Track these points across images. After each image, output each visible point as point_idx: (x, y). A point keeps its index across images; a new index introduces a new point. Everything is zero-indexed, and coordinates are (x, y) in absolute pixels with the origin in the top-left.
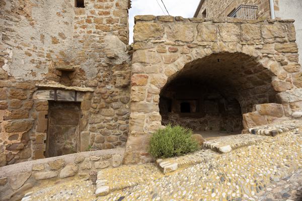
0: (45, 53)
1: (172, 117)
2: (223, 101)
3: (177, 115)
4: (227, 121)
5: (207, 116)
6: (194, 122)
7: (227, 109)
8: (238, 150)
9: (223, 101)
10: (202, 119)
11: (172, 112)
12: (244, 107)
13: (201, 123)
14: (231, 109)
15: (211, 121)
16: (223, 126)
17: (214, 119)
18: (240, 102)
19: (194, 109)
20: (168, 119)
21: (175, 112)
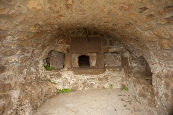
0: (25, 110)
1: (65, 75)
2: (127, 54)
3: (71, 73)
4: (130, 79)
5: (107, 72)
6: (92, 79)
7: (131, 64)
8: (134, 99)
9: (127, 54)
10: (102, 76)
11: (66, 69)
12: (158, 76)
13: (100, 79)
14: (135, 65)
15: (113, 77)
16: (125, 83)
17: (115, 75)
18: (150, 65)
19: (93, 63)
20: (60, 77)
21: (68, 69)
